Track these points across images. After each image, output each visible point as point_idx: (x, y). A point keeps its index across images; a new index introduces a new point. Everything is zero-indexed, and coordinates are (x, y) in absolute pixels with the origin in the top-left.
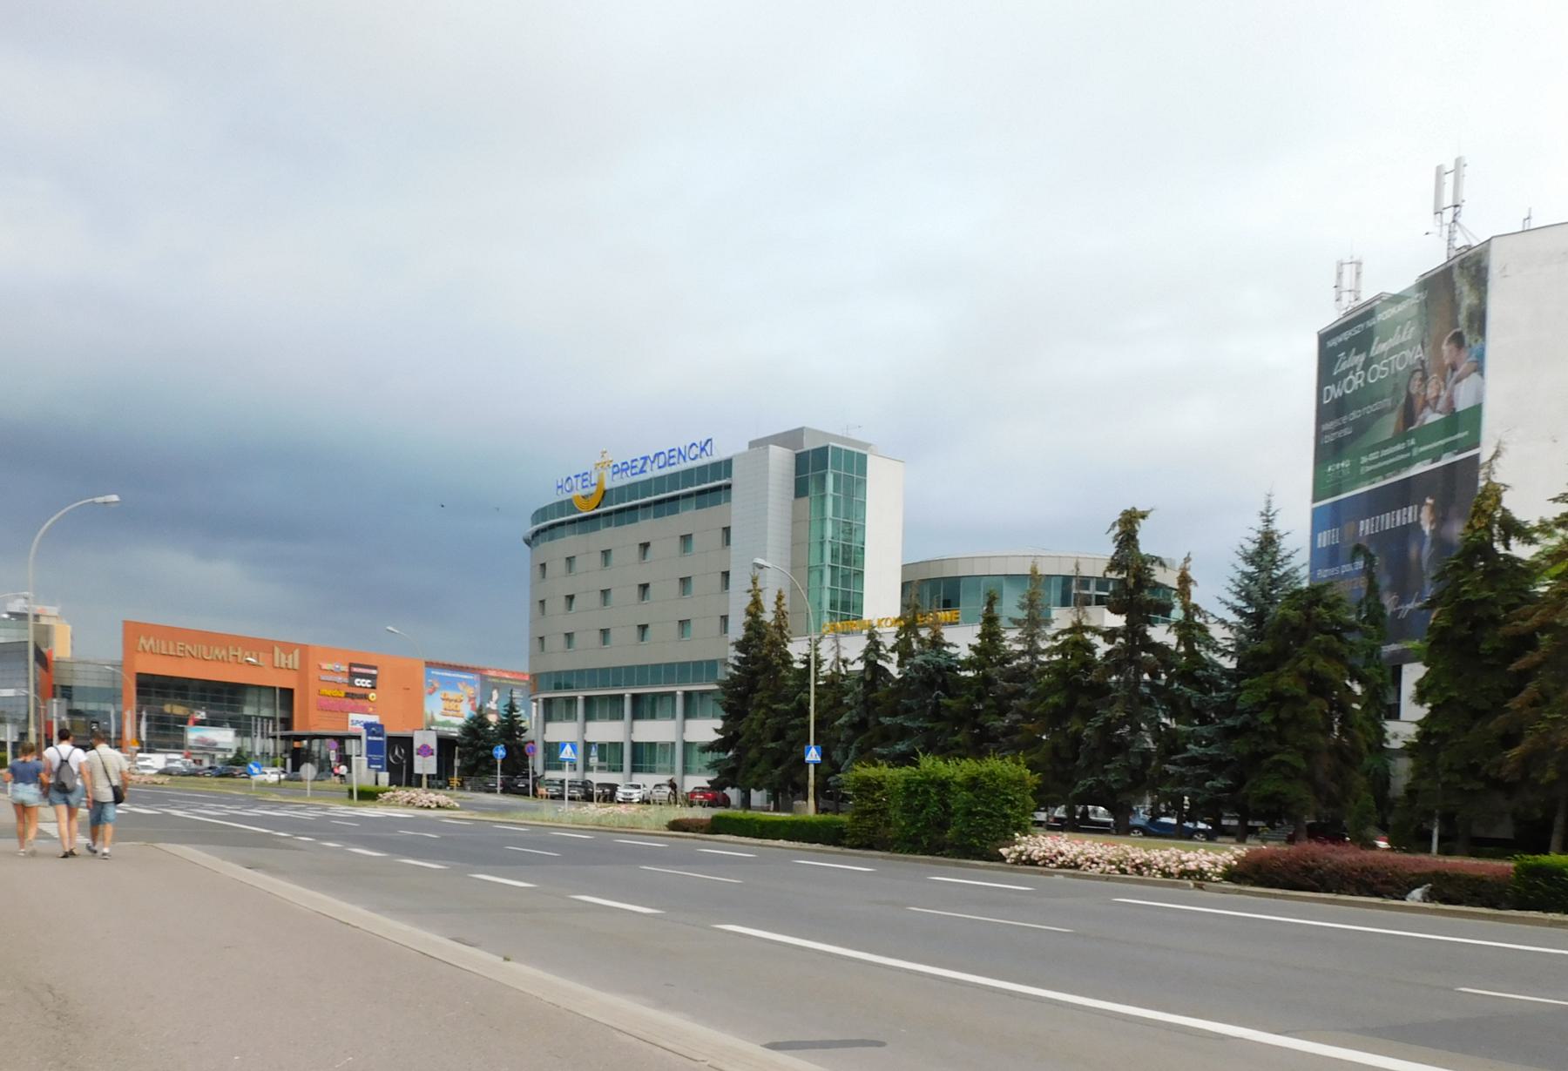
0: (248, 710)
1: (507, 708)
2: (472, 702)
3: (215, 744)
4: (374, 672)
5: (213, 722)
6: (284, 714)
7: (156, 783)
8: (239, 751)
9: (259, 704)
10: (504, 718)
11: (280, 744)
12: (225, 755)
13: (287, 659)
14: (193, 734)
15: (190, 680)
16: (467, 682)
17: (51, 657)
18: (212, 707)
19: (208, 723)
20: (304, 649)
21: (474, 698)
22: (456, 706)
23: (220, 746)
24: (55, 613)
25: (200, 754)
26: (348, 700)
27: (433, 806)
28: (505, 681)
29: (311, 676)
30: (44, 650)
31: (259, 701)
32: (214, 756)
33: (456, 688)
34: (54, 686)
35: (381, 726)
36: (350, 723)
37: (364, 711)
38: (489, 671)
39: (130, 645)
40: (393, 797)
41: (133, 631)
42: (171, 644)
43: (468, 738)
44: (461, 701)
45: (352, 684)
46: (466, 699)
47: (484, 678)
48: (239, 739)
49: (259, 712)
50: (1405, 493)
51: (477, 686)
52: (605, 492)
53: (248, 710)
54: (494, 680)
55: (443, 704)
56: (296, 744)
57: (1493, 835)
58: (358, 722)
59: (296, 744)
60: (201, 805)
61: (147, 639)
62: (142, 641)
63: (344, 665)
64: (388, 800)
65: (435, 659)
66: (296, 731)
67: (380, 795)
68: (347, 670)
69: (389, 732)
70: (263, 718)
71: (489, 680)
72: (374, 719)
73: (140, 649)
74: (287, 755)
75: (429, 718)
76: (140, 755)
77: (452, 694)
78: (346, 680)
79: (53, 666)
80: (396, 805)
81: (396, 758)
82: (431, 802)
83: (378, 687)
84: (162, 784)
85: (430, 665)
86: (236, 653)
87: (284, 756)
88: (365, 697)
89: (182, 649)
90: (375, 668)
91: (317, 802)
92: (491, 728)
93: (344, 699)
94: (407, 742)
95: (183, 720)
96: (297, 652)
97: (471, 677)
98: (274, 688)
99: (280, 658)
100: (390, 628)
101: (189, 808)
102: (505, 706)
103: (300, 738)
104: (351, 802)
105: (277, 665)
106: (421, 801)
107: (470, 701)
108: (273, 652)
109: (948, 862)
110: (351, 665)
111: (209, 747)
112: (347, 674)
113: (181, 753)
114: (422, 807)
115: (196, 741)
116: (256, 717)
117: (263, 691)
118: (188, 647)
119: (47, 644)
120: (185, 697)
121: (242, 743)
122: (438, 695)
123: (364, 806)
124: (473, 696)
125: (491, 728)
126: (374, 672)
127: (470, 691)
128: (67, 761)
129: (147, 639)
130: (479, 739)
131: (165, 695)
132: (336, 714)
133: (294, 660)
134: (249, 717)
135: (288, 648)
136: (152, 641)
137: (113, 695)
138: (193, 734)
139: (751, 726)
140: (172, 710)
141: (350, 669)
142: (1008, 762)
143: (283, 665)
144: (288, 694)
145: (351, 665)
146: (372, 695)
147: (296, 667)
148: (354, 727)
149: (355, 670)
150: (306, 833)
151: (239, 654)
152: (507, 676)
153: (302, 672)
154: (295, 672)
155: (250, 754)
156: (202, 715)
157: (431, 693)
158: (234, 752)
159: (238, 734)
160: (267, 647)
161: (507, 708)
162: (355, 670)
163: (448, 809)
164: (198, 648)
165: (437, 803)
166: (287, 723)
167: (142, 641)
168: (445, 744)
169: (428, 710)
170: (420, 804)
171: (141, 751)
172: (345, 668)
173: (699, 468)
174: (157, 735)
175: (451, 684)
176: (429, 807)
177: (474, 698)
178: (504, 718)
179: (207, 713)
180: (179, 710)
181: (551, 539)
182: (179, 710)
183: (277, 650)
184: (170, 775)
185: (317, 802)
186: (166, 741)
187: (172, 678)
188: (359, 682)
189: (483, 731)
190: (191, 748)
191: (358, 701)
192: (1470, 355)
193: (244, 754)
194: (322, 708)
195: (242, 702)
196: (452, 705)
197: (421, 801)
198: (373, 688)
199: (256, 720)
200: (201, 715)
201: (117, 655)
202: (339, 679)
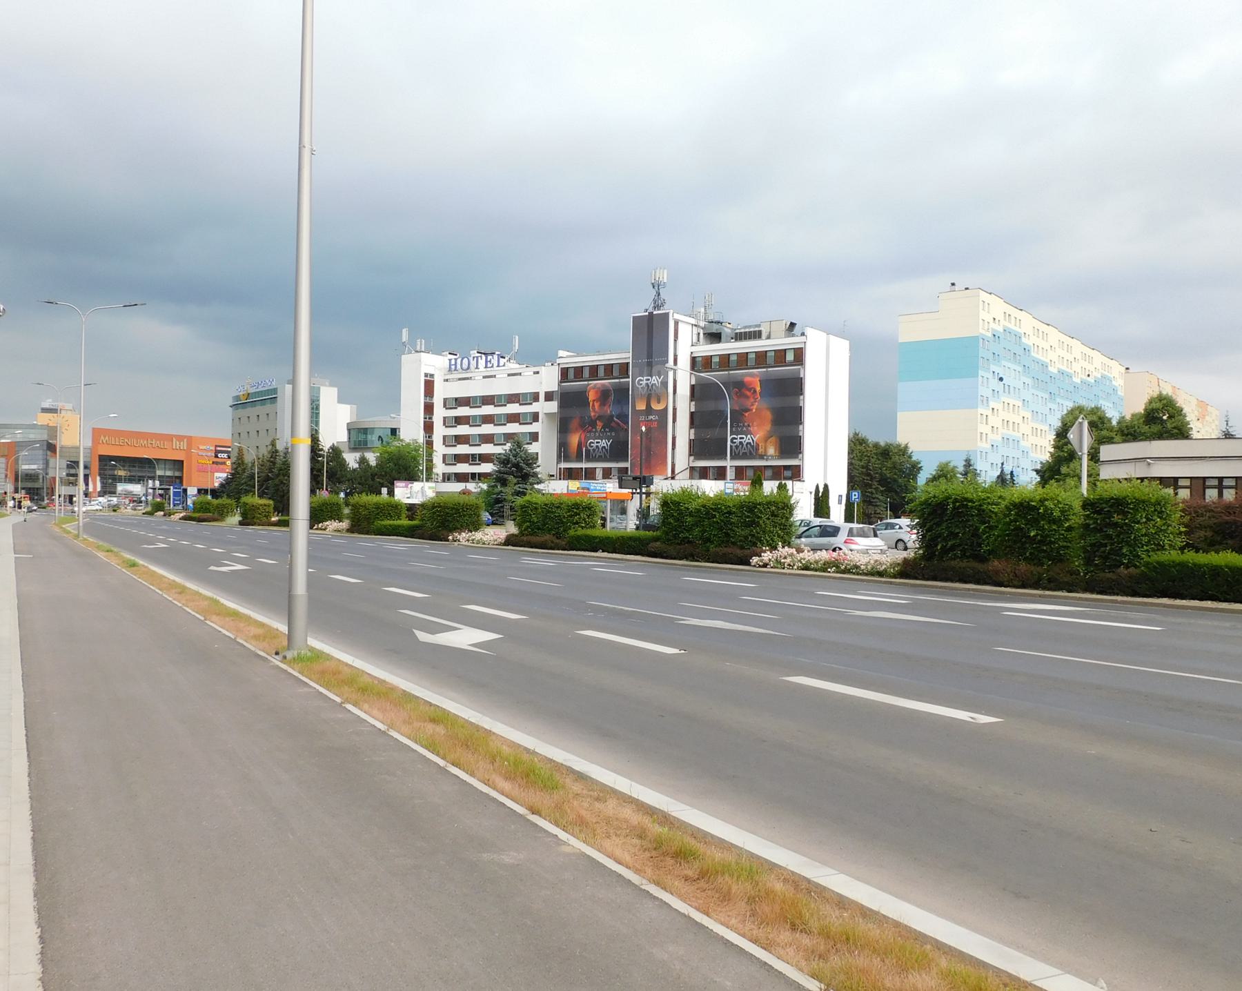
4: (230, 449)
9: (165, 469)
20: (190, 439)
41: (97, 433)
42: (162, 442)
45: (216, 456)
50: (1067, 505)
52: (249, 394)
58: (219, 477)
61: (105, 437)
62: (102, 438)
63: (212, 446)
73: (101, 442)
90: (229, 447)
96: (185, 440)
99: (176, 444)
105: (174, 447)
108: (172, 441)
109: (1022, 594)
110: (216, 446)
115: (122, 491)
117: (167, 462)
118: (126, 440)
126: (230, 449)
129: (105, 437)
133: (184, 445)
135: (180, 438)
136: (107, 438)
139: (120, 481)
142: (1071, 472)
143: (178, 448)
145: (216, 446)
147: (185, 448)
149: (219, 449)
150: (532, 566)
151: (153, 442)
153: (188, 451)
160: (169, 438)
162: (219, 449)
167: (102, 438)
172: (213, 448)
173: (265, 391)
181: (252, 407)
183: (174, 440)
191: (220, 466)
192: (1122, 519)
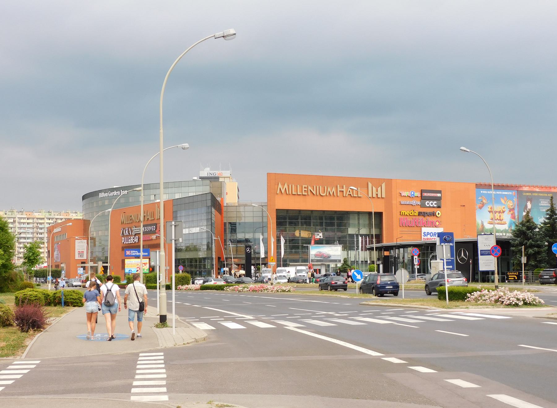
0: (351, 231)
1: (549, 212)
2: (511, 212)
3: (329, 257)
4: (439, 195)
5: (328, 241)
6: (374, 232)
7: (284, 291)
8: (345, 261)
10: (547, 221)
11: (375, 254)
12: (336, 265)
13: (377, 191)
14: (314, 251)
15: (312, 211)
16: (508, 197)
17: (223, 204)
18: (326, 230)
19: (324, 242)
20: (389, 182)
21: (513, 209)
22: (500, 216)
23: (332, 258)
24: (229, 175)
25: (319, 265)
26: (421, 218)
27: (521, 303)
28: (536, 194)
29: (394, 202)
30: (219, 199)
31: (359, 223)
32: (329, 266)
33: (499, 203)
34: (225, 224)
35: (451, 234)
36: (423, 234)
37: (433, 225)
38: (524, 187)
39: (271, 191)
40: (480, 296)
43: (519, 239)
44: (504, 212)
46: (507, 211)
47: (520, 193)
48: (346, 252)
49: (359, 230)
51: (515, 199)
53: (351, 231)
54: (528, 194)
55: (490, 215)
56: (386, 253)
57: (148, 263)
59: (386, 253)
60: (314, 314)
64: (476, 300)
65: (483, 182)
66: (385, 243)
67: (468, 295)
68: (419, 195)
69: (458, 238)
70: (361, 235)
71: (524, 194)
72: (441, 230)
74: (380, 262)
75: (480, 227)
76: (279, 268)
77: (497, 208)
78: (419, 203)
79: (224, 209)
80: (484, 304)
81: (462, 260)
82: (518, 299)
83: (442, 206)
84: (289, 291)
85: (479, 186)
86: (342, 190)
87: (378, 263)
88: (434, 214)
89: (306, 190)
90: (440, 192)
91: (414, 305)
92: (537, 230)
93: (418, 217)
94: (474, 244)
95: (308, 241)
97: (511, 193)
98: (370, 213)
99: (372, 190)
100: (463, 148)
101: (303, 317)
102: (548, 210)
103: (388, 248)
104: (442, 303)
106: (509, 299)
107: (510, 211)
110: (422, 192)
111: (325, 259)
112: (420, 198)
113: (307, 265)
114: (510, 305)
116: (357, 235)
119: (221, 194)
120: (309, 224)
121: (348, 255)
122: (486, 209)
123: (457, 306)
124: (511, 207)
125: (537, 230)
126: (439, 195)
127: (510, 204)
128: (110, 290)
130: (528, 239)
131: (296, 224)
132: (410, 229)
133: (382, 191)
134: (352, 236)
135: (377, 182)
137: (262, 227)
138: (314, 251)
140: (300, 234)
141: (421, 194)
144: (379, 215)
146: (438, 212)
148: (425, 237)
149: (425, 194)
151: (344, 190)
152: (537, 190)
153: (388, 199)
154: (383, 200)
155: (353, 262)
156: (319, 235)
157: (480, 208)
158: (342, 262)
159: (344, 248)
161: (549, 212)
162: (425, 194)
163: (534, 305)
164: (316, 187)
165: (524, 300)
166: (379, 238)
168: (501, 243)
169: (479, 221)
170: (508, 302)
171: (279, 265)
172: (418, 194)
174: (291, 253)
175: (497, 200)
176: (516, 305)
177: (513, 209)
178: (547, 221)
179: (323, 234)
180: (305, 234)
182: (305, 234)
184: (298, 282)
185: (414, 305)
186: (296, 257)
187: (300, 211)
188: (428, 204)
189: (531, 232)
190: (312, 261)
191: (428, 217)
193: (349, 263)
194: (402, 225)
195: (347, 226)
196: (497, 216)
197: (509, 299)
198: (439, 207)
199: (357, 238)
200: (319, 235)
201: (264, 199)
202: (414, 202)
